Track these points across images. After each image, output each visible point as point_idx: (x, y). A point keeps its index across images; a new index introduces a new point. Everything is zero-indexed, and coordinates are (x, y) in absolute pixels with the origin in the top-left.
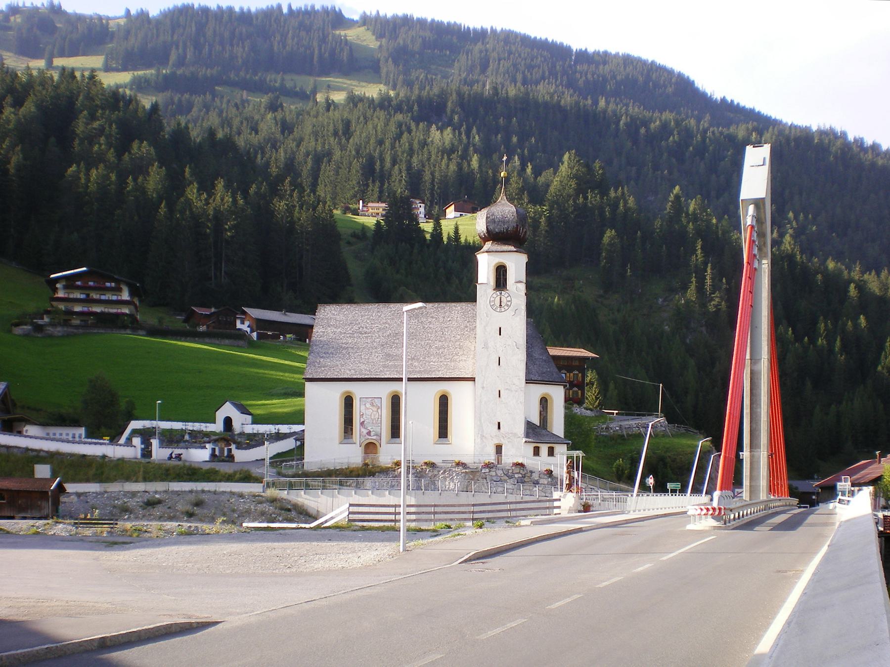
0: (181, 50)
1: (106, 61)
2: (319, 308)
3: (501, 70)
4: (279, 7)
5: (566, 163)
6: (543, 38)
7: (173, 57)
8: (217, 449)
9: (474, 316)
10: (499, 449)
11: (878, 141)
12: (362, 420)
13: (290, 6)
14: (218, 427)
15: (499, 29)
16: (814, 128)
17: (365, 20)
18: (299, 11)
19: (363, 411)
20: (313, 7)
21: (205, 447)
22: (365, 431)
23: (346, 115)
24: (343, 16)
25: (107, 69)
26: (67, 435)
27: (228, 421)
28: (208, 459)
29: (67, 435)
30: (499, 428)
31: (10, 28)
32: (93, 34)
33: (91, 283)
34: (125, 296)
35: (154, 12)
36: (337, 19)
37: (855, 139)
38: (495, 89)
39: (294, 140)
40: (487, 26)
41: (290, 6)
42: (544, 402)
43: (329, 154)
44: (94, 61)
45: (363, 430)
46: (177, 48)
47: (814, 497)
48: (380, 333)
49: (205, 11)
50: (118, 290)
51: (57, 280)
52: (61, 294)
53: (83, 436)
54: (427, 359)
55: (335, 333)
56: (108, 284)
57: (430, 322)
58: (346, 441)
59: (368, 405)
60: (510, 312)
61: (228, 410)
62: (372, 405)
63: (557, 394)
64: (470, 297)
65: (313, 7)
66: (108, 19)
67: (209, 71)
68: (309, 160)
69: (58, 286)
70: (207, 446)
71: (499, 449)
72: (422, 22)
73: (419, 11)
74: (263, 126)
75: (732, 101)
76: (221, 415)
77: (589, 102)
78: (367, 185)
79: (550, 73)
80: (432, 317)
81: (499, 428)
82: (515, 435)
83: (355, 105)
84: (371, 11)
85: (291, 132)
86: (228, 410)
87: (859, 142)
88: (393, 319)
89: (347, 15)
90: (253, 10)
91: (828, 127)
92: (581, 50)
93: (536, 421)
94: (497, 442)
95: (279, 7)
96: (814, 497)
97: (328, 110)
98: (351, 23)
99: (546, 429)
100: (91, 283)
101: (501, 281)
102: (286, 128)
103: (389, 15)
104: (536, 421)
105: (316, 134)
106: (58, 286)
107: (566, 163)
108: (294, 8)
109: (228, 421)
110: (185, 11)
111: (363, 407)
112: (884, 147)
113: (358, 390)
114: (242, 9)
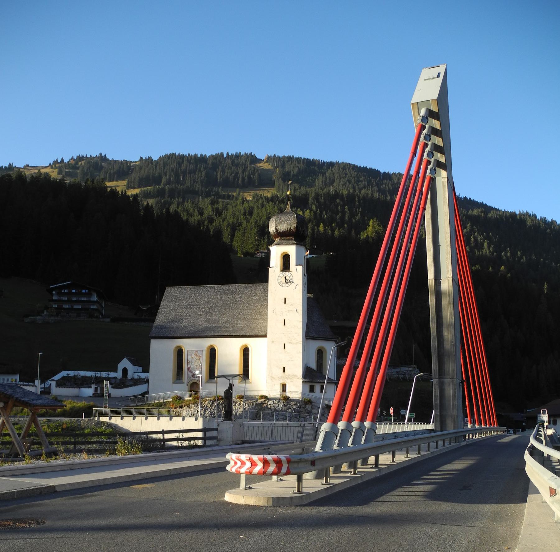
0: (168, 177)
1: (128, 183)
2: (167, 289)
3: (342, 183)
4: (222, 154)
5: (371, 226)
6: (365, 166)
7: (164, 180)
8: (99, 388)
9: (266, 291)
10: (284, 387)
11: (554, 219)
12: (189, 366)
13: (228, 153)
14: (118, 375)
15: (340, 162)
16: (517, 213)
17: (269, 159)
18: (233, 155)
19: (190, 360)
20: (240, 153)
21: (91, 387)
22: (190, 374)
23: (251, 205)
24: (256, 158)
25: (129, 187)
26: (4, 379)
27: (125, 371)
28: (92, 395)
29: (4, 379)
30: (284, 371)
31: (78, 168)
32: (123, 170)
33: (74, 291)
34: (95, 298)
35: (155, 158)
36: (253, 159)
37: (541, 218)
38: (336, 191)
39: (221, 218)
40: (334, 161)
41: (228, 153)
42: (320, 353)
43: (240, 225)
44: (124, 183)
45: (189, 373)
46: (166, 176)
47: (524, 424)
48: (206, 305)
49: (182, 157)
50: (89, 294)
51: (54, 289)
52: (55, 298)
53: (18, 380)
54: (236, 322)
55: (175, 305)
56: (84, 291)
57: (241, 297)
58: (178, 381)
59: (193, 355)
60: (293, 286)
61: (125, 363)
62: (196, 355)
63: (331, 349)
64: (264, 279)
65: (240, 153)
66: (131, 162)
67: (182, 187)
68: (229, 229)
69: (54, 292)
70: (92, 386)
71: (284, 387)
72: (298, 160)
73: (297, 154)
74: (206, 212)
75: (470, 199)
76: (120, 367)
77: (389, 198)
78: (260, 241)
79: (368, 185)
80: (243, 294)
81: (284, 371)
82: (296, 376)
83: (258, 200)
84: (271, 153)
85: (220, 214)
86: (125, 363)
87: (544, 220)
88: (215, 295)
89: (258, 157)
90: (208, 155)
91: (525, 212)
92: (385, 173)
93: (314, 366)
94: (282, 382)
95: (222, 154)
96: (524, 424)
97: (243, 203)
98: (261, 161)
99: (322, 373)
100: (74, 291)
101: (286, 266)
102: (219, 212)
103: (281, 156)
104: (314, 366)
105: (234, 215)
106: (54, 292)
107: (371, 226)
108: (230, 154)
109: (125, 371)
110: (171, 157)
111: (189, 357)
112: (558, 223)
113: (187, 344)
114: (201, 155)
